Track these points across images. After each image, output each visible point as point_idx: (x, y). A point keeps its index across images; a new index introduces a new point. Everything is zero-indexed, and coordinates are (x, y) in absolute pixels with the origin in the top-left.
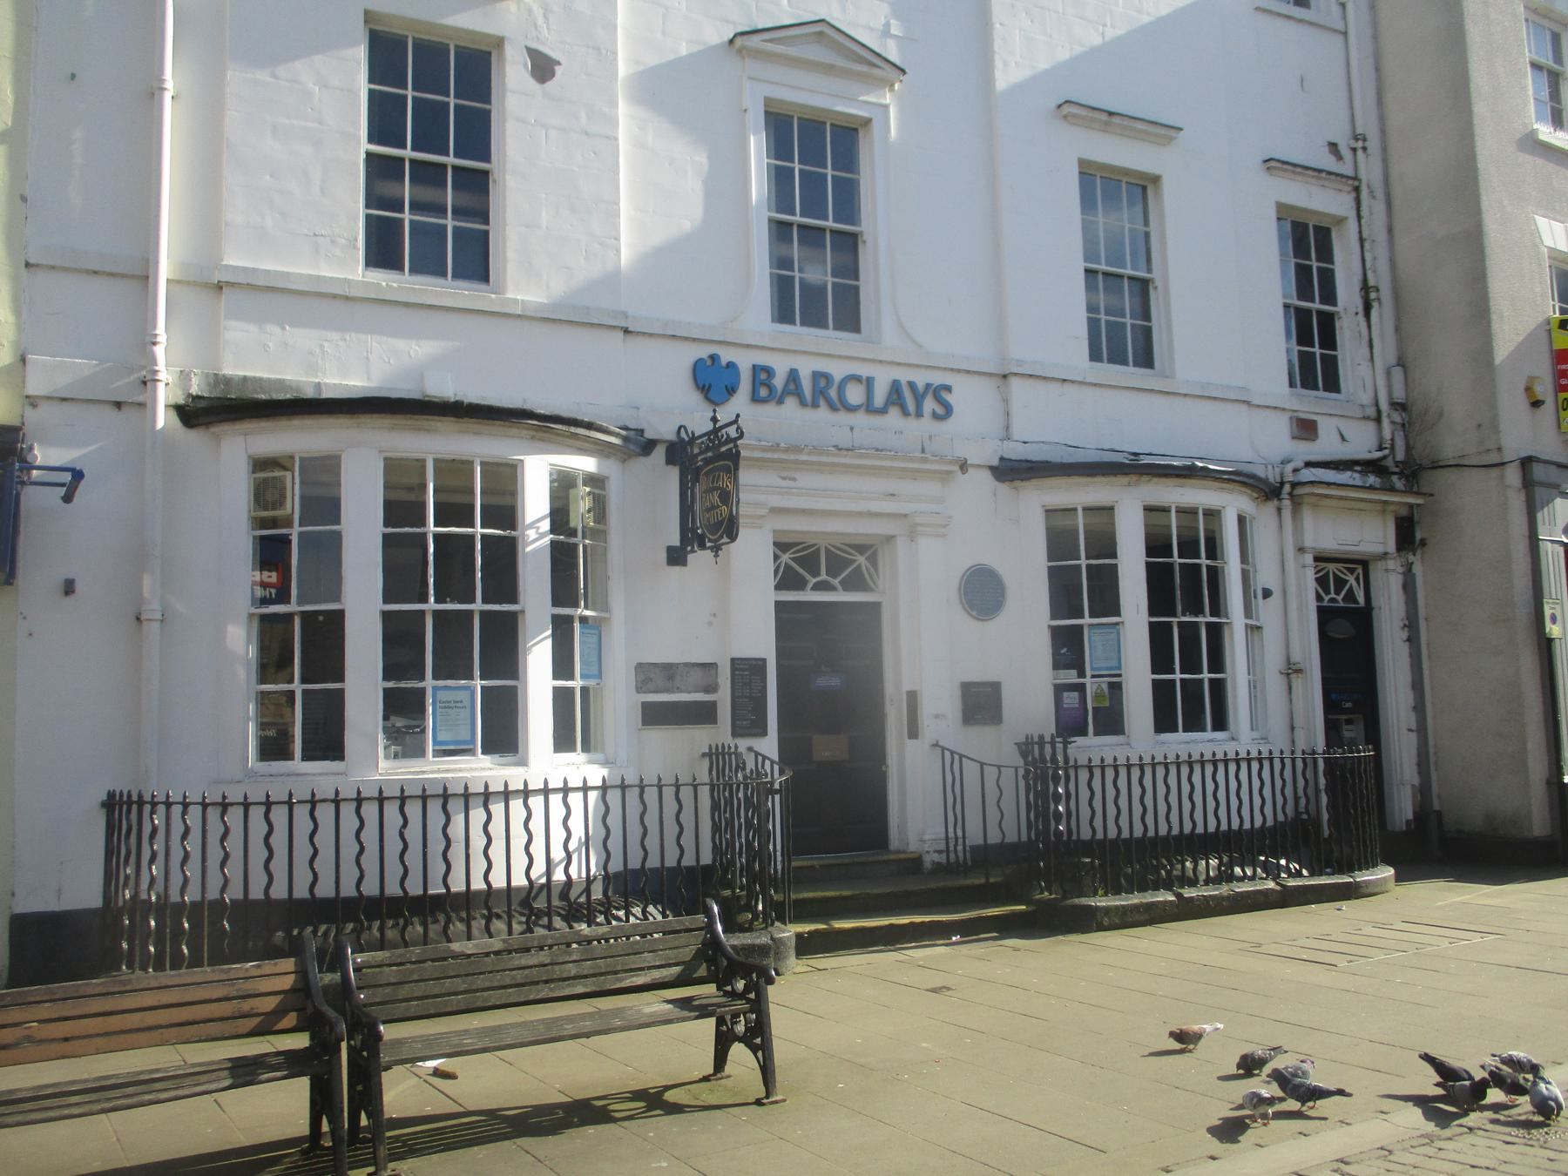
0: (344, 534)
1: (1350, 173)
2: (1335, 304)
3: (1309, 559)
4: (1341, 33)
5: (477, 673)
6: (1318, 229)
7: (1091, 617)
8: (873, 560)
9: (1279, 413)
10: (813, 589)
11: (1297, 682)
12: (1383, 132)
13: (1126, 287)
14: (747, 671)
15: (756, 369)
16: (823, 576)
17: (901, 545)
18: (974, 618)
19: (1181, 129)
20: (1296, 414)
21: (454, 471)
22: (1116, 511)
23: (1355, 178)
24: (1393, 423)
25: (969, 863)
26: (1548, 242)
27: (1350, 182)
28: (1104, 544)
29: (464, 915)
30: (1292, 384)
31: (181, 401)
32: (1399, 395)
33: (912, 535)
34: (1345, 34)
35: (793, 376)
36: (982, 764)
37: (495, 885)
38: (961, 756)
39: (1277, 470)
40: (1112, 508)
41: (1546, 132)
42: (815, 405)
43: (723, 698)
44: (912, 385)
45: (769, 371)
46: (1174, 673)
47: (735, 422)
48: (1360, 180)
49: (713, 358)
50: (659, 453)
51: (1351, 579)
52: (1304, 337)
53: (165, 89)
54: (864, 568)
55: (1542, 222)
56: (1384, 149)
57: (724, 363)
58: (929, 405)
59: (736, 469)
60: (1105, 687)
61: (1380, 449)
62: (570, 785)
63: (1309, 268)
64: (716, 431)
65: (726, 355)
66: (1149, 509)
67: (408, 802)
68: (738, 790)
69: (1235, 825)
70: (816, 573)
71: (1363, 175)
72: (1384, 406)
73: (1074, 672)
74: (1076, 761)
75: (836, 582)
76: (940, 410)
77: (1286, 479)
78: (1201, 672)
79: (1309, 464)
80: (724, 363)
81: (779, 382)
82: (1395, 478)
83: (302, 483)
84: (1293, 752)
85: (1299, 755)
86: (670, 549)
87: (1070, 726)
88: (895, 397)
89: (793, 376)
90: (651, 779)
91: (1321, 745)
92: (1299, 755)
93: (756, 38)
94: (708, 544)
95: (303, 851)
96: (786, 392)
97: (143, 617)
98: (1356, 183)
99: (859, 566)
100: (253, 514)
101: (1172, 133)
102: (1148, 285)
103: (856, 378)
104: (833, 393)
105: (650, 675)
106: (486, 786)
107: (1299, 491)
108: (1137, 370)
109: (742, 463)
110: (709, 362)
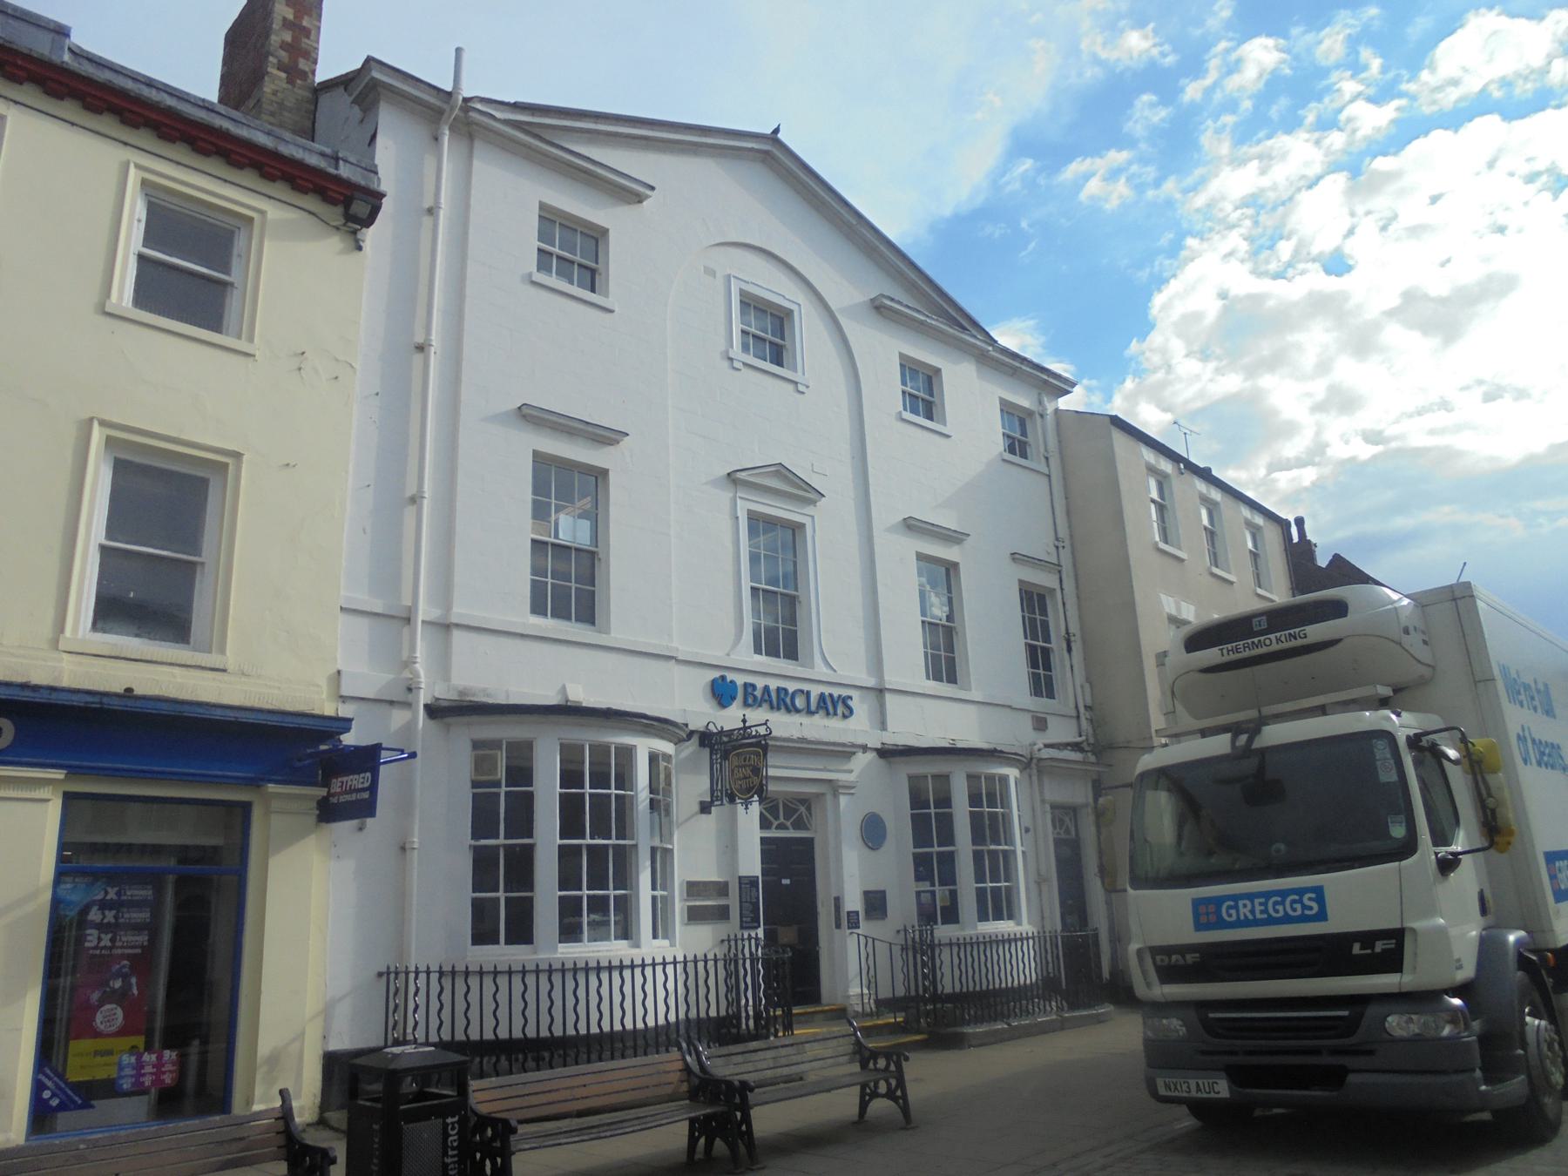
0: (535, 793)
1: (1055, 561)
2: (1050, 643)
3: (1048, 808)
4: (1047, 475)
5: (611, 885)
6: (1038, 595)
7: (938, 846)
8: (809, 809)
9: (1026, 713)
10: (777, 828)
11: (1045, 888)
12: (1071, 536)
13: (573, 556)
14: (748, 883)
15: (746, 685)
16: (782, 819)
17: (829, 797)
18: (869, 847)
19: (628, 435)
20: (1035, 714)
21: (600, 751)
22: (951, 777)
23: (1059, 565)
24: (1087, 719)
25: (874, 1009)
26: (1167, 610)
27: (1057, 567)
28: (521, 773)
29: (561, 1052)
30: (1031, 695)
31: (429, 702)
32: (1089, 703)
33: (836, 795)
34: (1049, 476)
35: (766, 689)
36: (890, 944)
37: (556, 1034)
38: (873, 939)
39: (1028, 751)
40: (948, 776)
41: (1162, 546)
42: (779, 709)
43: (733, 902)
44: (831, 695)
45: (753, 686)
46: (498, 899)
47: (766, 724)
48: (1061, 566)
49: (723, 678)
50: (695, 740)
51: (1067, 819)
52: (1034, 663)
53: (424, 497)
54: (805, 817)
55: (1163, 596)
56: (1072, 545)
57: (728, 680)
58: (840, 709)
59: (765, 755)
60: (947, 893)
61: (1080, 736)
62: (527, 969)
63: (1035, 619)
64: (745, 728)
65: (730, 676)
66: (477, 745)
67: (527, 975)
68: (730, 965)
69: (984, 987)
70: (777, 818)
71: (1063, 563)
72: (1082, 710)
73: (928, 883)
74: (940, 941)
75: (788, 824)
76: (847, 713)
77: (1034, 756)
78: (498, 899)
79: (1047, 746)
80: (728, 680)
81: (758, 693)
82: (1089, 754)
83: (507, 757)
84: (1044, 932)
85: (1047, 934)
86: (702, 803)
87: (927, 916)
88: (822, 704)
89: (766, 689)
90: (700, 956)
91: (1059, 927)
92: (1047, 934)
93: (744, 474)
94: (738, 801)
95: (518, 1005)
96: (763, 700)
97: (407, 846)
98: (1060, 568)
99: (801, 815)
100: (473, 777)
101: (964, 537)
102: (951, 631)
103: (802, 691)
104: (788, 700)
105: (693, 888)
106: (610, 962)
107: (1042, 764)
108: (579, 625)
109: (769, 748)
110: (720, 681)
